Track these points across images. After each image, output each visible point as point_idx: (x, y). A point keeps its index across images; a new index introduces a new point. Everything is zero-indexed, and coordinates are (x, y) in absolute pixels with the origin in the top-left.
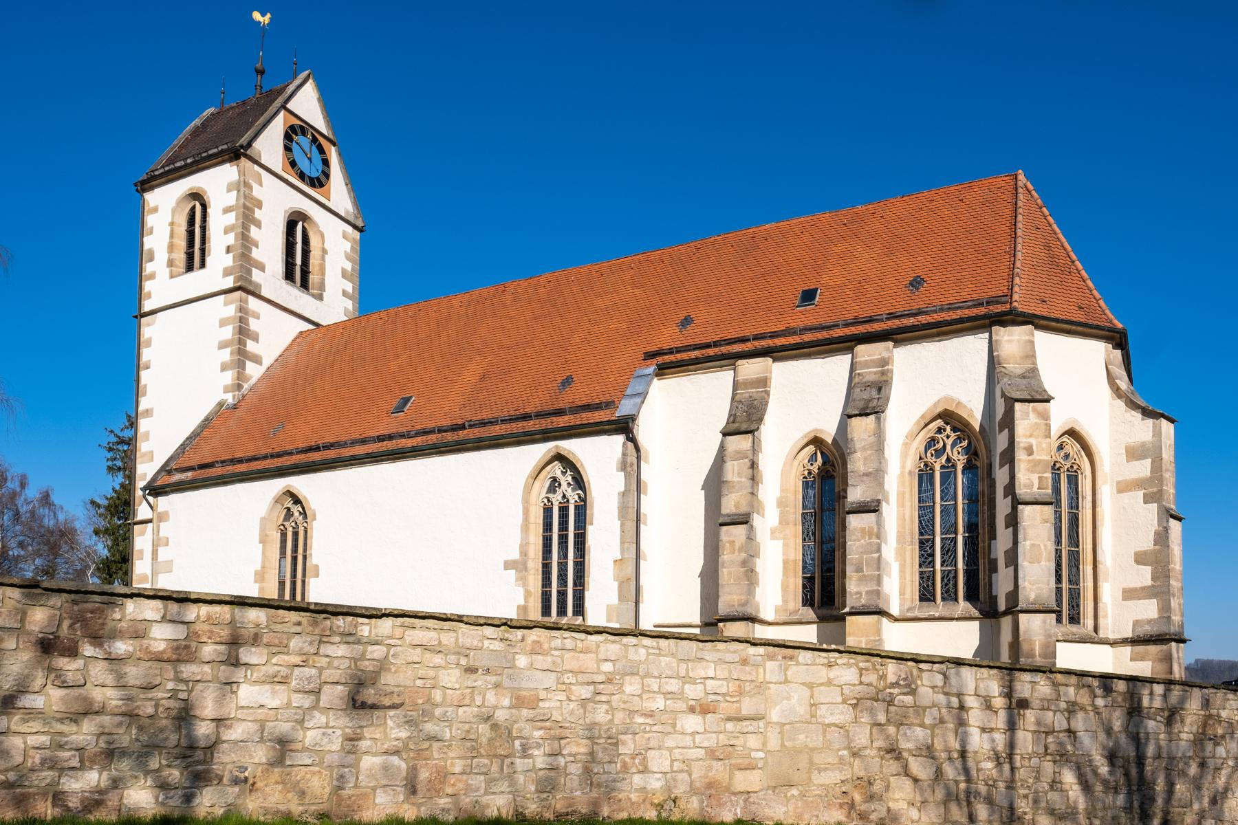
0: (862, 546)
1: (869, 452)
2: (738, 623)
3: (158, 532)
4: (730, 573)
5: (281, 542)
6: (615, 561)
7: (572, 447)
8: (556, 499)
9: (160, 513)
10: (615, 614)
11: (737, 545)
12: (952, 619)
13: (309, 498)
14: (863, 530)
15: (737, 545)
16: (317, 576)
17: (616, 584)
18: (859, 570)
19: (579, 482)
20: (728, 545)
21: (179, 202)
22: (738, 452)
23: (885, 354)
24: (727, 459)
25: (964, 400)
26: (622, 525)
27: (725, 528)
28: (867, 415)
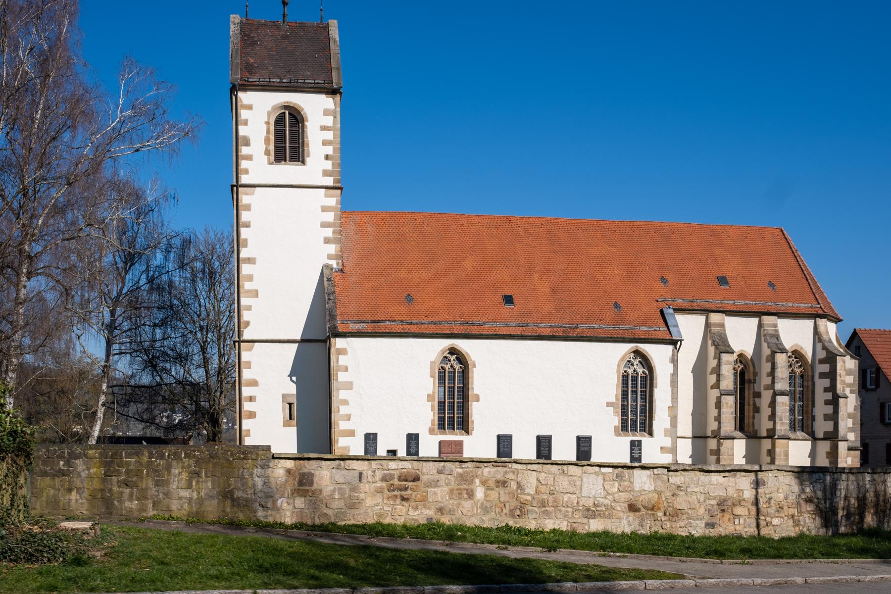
0: (782, 410)
1: (783, 369)
2: (729, 440)
3: (338, 361)
4: (726, 417)
5: (673, 398)
6: (669, 407)
7: (646, 348)
8: (630, 371)
9: (338, 349)
10: (669, 433)
11: (729, 405)
12: (798, 440)
13: (469, 352)
14: (783, 403)
15: (729, 405)
16: (478, 400)
17: (669, 418)
18: (781, 420)
19: (651, 369)
20: (725, 404)
21: (274, 108)
22: (728, 361)
23: (775, 322)
24: (722, 364)
25: (804, 346)
26: (672, 390)
27: (724, 396)
28: (783, 353)
